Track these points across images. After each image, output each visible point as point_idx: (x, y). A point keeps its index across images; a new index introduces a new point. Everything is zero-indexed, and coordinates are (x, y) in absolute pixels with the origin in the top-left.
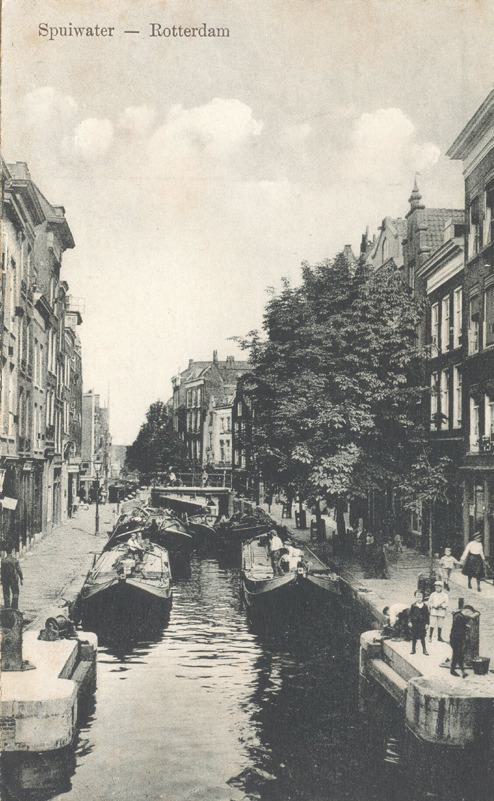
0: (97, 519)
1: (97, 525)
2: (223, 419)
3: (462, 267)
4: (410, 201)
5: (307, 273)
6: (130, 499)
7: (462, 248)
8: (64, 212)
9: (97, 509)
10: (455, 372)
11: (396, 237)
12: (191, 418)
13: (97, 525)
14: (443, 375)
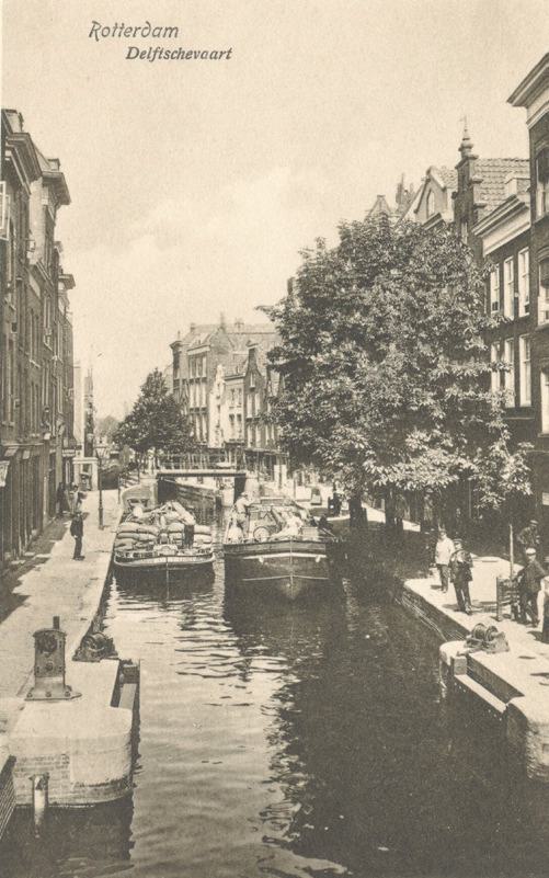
0: (101, 510)
1: (101, 517)
2: (233, 391)
3: (528, 227)
4: (460, 150)
5: (345, 235)
6: (131, 484)
7: (528, 205)
8: (59, 165)
9: (101, 495)
10: (522, 342)
11: (444, 190)
12: (195, 394)
13: (101, 517)
14: (507, 346)
